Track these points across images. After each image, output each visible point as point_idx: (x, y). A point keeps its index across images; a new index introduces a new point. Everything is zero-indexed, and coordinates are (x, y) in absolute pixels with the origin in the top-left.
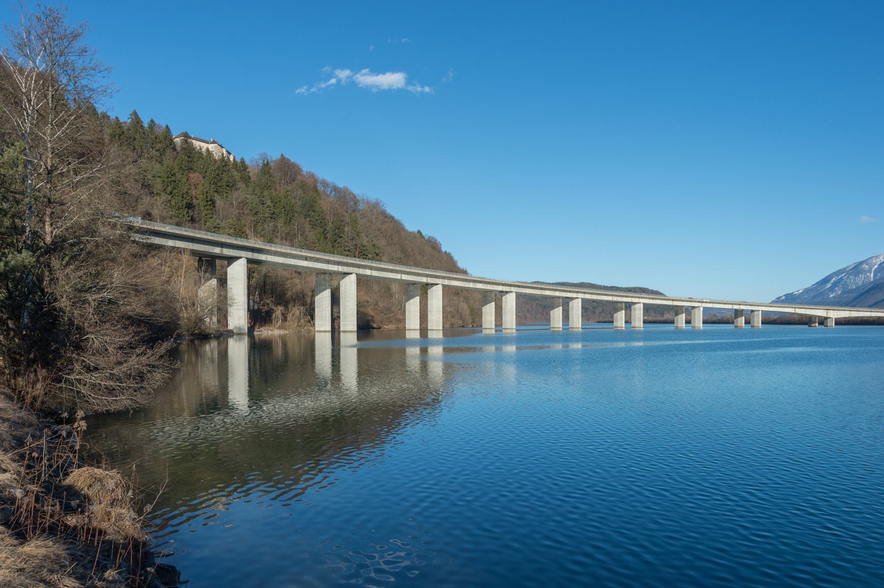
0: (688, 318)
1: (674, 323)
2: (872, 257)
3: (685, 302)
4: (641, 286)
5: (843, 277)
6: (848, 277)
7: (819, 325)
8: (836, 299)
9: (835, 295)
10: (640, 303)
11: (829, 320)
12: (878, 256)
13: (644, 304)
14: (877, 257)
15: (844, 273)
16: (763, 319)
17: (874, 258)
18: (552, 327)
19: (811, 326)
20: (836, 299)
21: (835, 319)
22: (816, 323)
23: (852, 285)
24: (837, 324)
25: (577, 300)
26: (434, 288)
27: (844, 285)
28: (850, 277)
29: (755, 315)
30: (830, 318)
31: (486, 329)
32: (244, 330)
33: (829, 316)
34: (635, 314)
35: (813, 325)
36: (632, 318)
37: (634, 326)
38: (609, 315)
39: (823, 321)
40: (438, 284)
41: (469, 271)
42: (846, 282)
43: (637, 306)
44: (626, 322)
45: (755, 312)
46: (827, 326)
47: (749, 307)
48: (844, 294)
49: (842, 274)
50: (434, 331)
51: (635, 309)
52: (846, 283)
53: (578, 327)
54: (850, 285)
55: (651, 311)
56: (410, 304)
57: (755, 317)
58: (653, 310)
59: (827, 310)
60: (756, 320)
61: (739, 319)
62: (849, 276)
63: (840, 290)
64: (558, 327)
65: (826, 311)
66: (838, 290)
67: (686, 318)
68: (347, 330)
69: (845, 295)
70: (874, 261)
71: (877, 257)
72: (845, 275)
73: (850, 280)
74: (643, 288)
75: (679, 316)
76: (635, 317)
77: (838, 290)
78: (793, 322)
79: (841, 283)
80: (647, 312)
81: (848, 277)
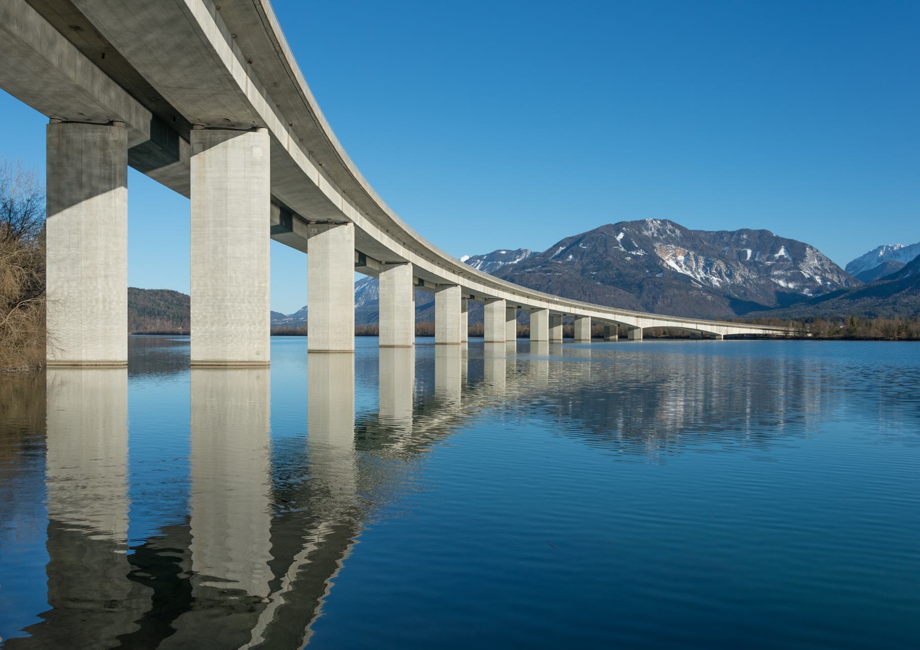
1: (304, 334)
4: (170, 289)
6: (370, 287)
15: (366, 283)
16: (357, 332)
18: (441, 341)
19: (609, 340)
22: (616, 335)
33: (638, 326)
34: (492, 318)
35: (611, 338)
38: (133, 325)
42: (369, 292)
45: (583, 319)
50: (331, 356)
51: (492, 311)
52: (368, 294)
57: (582, 326)
62: (371, 286)
63: (363, 301)
66: (361, 301)
67: (563, 330)
68: (230, 358)
69: (370, 306)
73: (372, 290)
77: (361, 301)
78: (857, 337)
79: (364, 293)
80: (181, 320)
81: (370, 287)
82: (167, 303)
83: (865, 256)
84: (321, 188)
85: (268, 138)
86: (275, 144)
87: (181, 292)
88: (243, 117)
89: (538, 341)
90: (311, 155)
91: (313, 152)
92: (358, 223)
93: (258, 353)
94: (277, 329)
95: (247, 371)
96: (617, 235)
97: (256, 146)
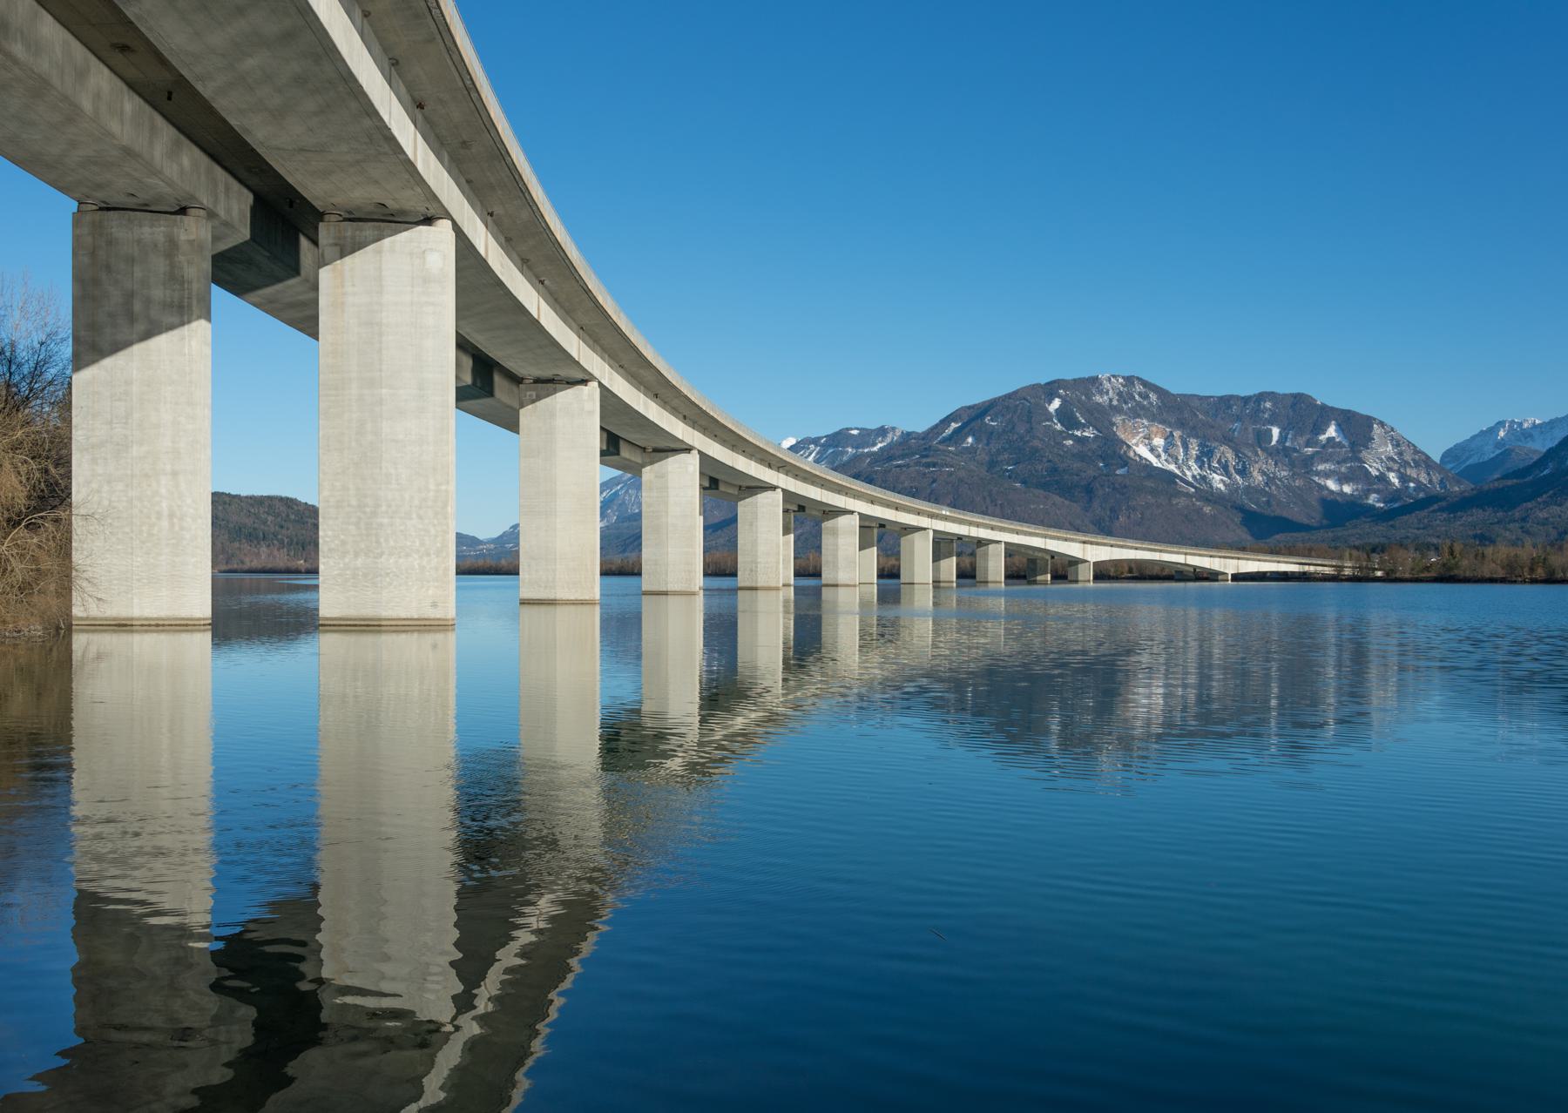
4: (284, 495)
5: (618, 491)
6: (627, 491)
7: (1053, 578)
8: (611, 531)
9: (607, 524)
11: (1081, 566)
15: (619, 484)
19: (1035, 582)
20: (611, 531)
23: (633, 505)
24: (1099, 577)
27: (620, 505)
28: (630, 491)
29: (990, 552)
31: (666, 593)
35: (1039, 578)
41: (888, 424)
48: (623, 522)
49: (617, 485)
50: (559, 608)
53: (998, 580)
54: (630, 507)
66: (611, 514)
68: (386, 612)
69: (626, 524)
72: (621, 488)
73: (630, 496)
74: (288, 498)
76: (835, 556)
77: (611, 514)
79: (615, 502)
82: (279, 519)
83: (1473, 438)
84: (543, 322)
85: (451, 236)
86: (464, 247)
87: (303, 501)
88: (409, 200)
89: (913, 584)
90: (525, 264)
91: (528, 260)
92: (603, 382)
93: (434, 605)
94: (468, 563)
95: (416, 635)
96: (1050, 403)
97: (431, 250)
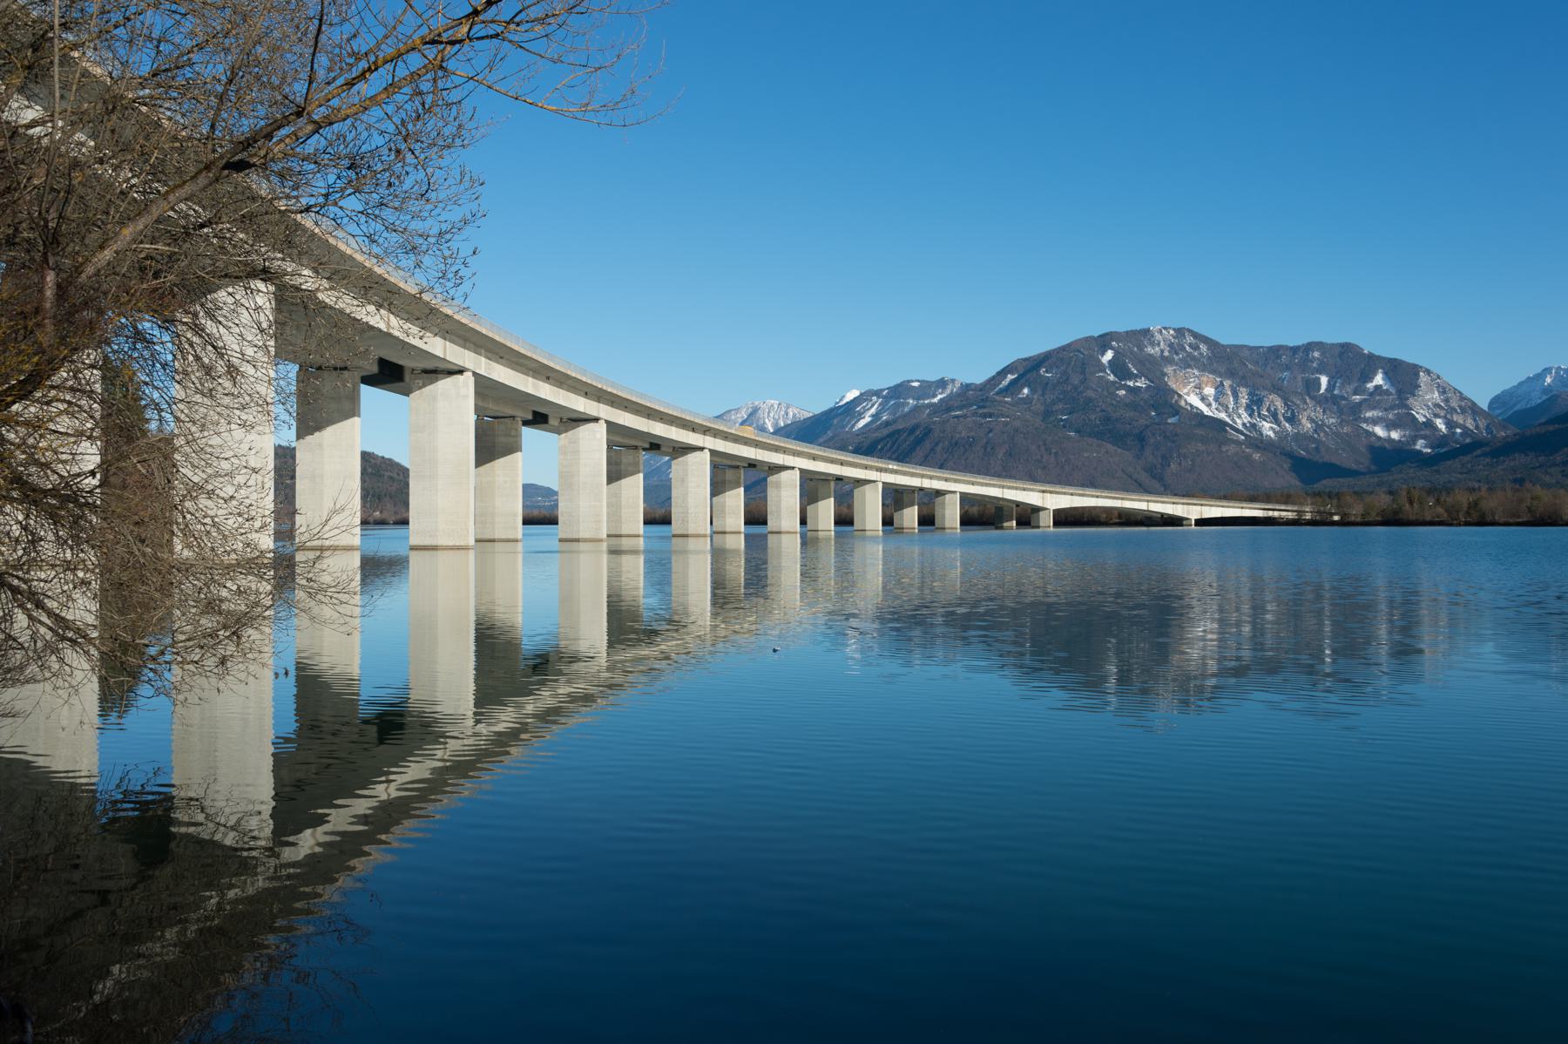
0: (845, 510)
2: (729, 411)
3: (858, 470)
7: (1017, 524)
10: (793, 468)
12: (739, 409)
13: (804, 473)
14: (737, 410)
17: (733, 412)
19: (1002, 528)
21: (1054, 510)
22: (1011, 520)
24: (1057, 523)
25: (697, 454)
26: (445, 384)
29: (947, 501)
30: (1046, 509)
31: (434, 548)
32: (637, 589)
33: (1045, 506)
35: (1005, 524)
36: (771, 508)
37: (720, 529)
39: (1027, 516)
40: (461, 372)
43: (784, 475)
44: (838, 522)
46: (1038, 527)
47: (943, 483)
50: (439, 553)
51: (778, 486)
55: (387, 499)
56: (320, 446)
58: (391, 498)
59: (1043, 492)
60: (948, 513)
61: (907, 511)
64: (860, 529)
65: (1041, 494)
70: (733, 417)
71: (737, 410)
75: (821, 503)
